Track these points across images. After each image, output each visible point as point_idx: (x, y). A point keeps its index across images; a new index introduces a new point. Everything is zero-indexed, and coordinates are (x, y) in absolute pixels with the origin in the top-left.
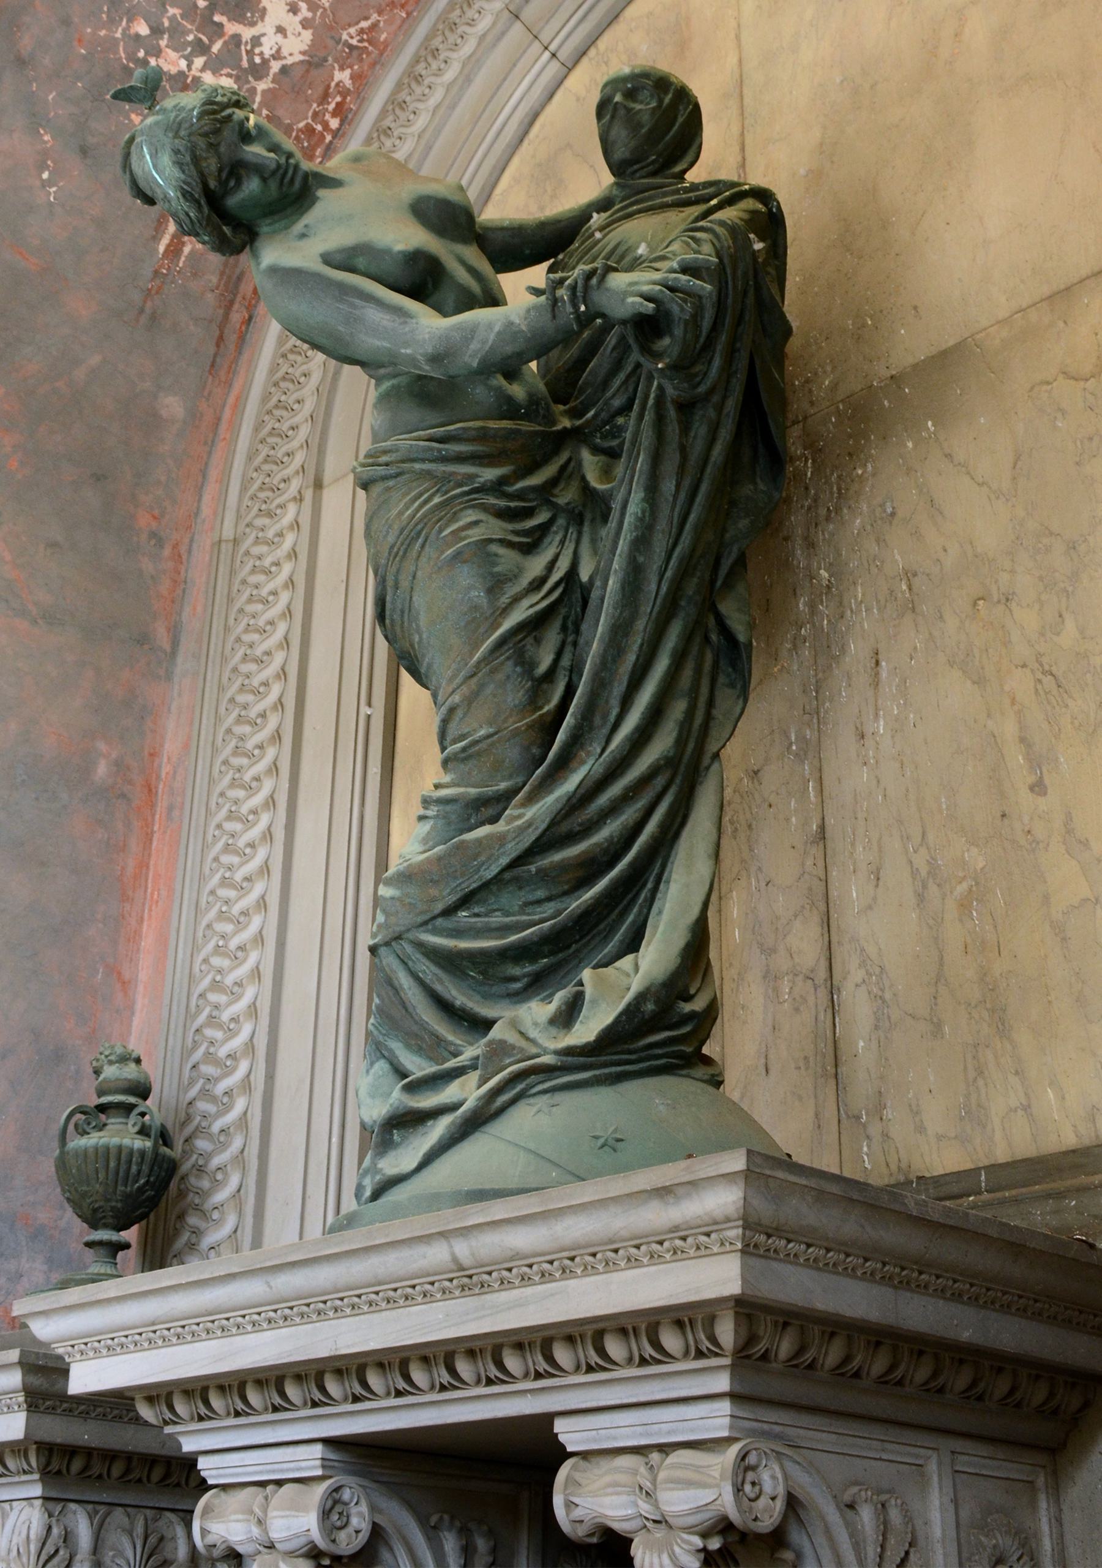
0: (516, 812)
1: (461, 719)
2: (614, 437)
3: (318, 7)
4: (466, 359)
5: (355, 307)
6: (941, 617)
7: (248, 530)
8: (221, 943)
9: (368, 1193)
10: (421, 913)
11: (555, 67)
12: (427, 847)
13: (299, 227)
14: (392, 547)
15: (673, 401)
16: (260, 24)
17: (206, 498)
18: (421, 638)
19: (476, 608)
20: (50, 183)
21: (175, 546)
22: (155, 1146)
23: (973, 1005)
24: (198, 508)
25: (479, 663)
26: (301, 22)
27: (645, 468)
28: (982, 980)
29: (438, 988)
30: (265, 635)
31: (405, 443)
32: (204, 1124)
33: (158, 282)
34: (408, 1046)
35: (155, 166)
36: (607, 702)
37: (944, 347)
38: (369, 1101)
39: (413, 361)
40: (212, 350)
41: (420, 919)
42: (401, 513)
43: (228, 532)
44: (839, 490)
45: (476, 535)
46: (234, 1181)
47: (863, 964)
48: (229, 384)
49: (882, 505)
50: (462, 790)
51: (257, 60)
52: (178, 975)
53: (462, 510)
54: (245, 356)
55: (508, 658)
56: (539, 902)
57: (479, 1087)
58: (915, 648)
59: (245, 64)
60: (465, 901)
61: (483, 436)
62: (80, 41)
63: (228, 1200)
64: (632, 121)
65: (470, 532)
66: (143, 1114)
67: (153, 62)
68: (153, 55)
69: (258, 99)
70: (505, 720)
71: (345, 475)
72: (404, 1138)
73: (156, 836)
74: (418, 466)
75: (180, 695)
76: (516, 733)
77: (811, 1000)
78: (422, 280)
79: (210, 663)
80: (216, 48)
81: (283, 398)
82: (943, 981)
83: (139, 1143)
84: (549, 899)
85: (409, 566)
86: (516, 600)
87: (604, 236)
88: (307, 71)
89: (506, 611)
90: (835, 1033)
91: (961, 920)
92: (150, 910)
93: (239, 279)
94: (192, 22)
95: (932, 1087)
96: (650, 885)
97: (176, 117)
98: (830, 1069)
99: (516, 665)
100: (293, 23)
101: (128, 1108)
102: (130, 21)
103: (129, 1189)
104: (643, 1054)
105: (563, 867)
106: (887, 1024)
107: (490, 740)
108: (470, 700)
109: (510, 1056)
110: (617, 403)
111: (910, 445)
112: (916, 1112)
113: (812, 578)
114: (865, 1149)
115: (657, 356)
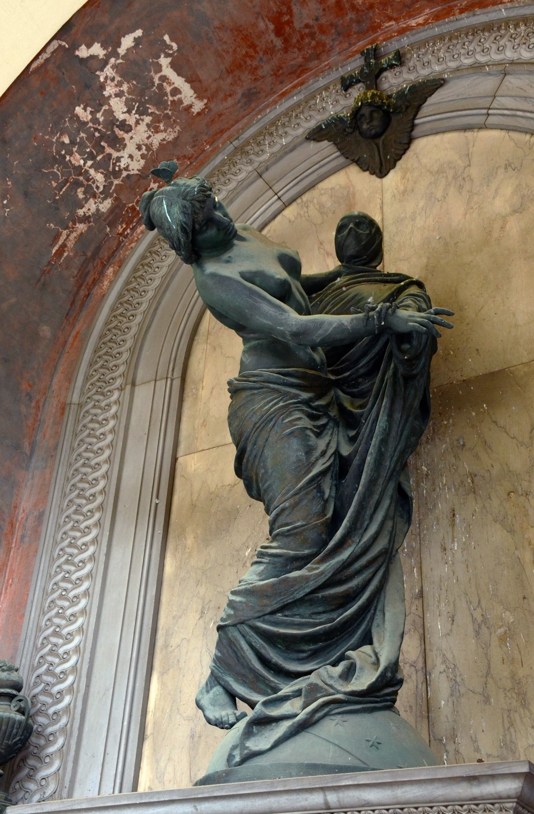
0: (315, 566)
1: (288, 515)
2: (355, 388)
3: (151, 150)
4: (314, 338)
5: (257, 302)
6: (490, 498)
7: (88, 400)
8: (60, 611)
9: (237, 759)
10: (259, 611)
11: (279, 204)
12: (261, 578)
13: (225, 256)
14: (256, 424)
15: (402, 375)
16: (122, 151)
17: (55, 380)
18: (266, 472)
19: (300, 461)
20: (6, 206)
21: (38, 402)
22: (27, 719)
23: (507, 689)
24: (50, 385)
25: (301, 489)
26: (141, 155)
27: (388, 405)
28: (512, 677)
29: (263, 651)
30: (97, 455)
31: (266, 373)
32: (43, 709)
33: (49, 267)
34: (236, 680)
35: (169, 212)
36: (363, 517)
37: (493, 370)
38: (210, 707)
39: (283, 334)
40: (68, 307)
41: (257, 615)
42: (261, 407)
43: (75, 399)
44: (434, 430)
45: (301, 424)
46: (60, 741)
47: (444, 662)
48: (73, 326)
49: (458, 440)
50: (285, 551)
51: (117, 169)
52: (30, 626)
53: (293, 411)
54: (84, 313)
55: (314, 488)
56: (319, 613)
57: (304, 708)
58: (475, 511)
59: (111, 169)
60: (280, 610)
61: (303, 376)
62: (35, 138)
63: (55, 752)
64: (358, 237)
65: (298, 423)
66: (20, 701)
67: (68, 158)
68: (68, 155)
69: (113, 188)
70: (311, 519)
71: (149, 382)
72: (259, 731)
73: (12, 551)
74: (272, 386)
75: (32, 478)
76: (316, 526)
77: (414, 677)
78: (283, 293)
79: (61, 464)
80: (99, 158)
81: (114, 337)
82: (490, 676)
83: (19, 717)
84: (324, 612)
85: (264, 434)
86: (317, 460)
87: (347, 290)
88: (139, 180)
89: (313, 464)
90: (427, 695)
91: (500, 647)
92: (6, 589)
93: (87, 274)
94: (91, 143)
95: (484, 729)
96: (372, 611)
97: (185, 189)
98: (425, 713)
99: (317, 492)
100: (137, 154)
101: (11, 697)
102: (61, 135)
103: (10, 742)
104: (382, 699)
105: (335, 597)
106: (458, 694)
107: (303, 528)
108: (294, 507)
109: (321, 692)
110: (362, 371)
111: (474, 414)
112: (474, 741)
113: (417, 469)
114: (445, 757)
115: (404, 352)
